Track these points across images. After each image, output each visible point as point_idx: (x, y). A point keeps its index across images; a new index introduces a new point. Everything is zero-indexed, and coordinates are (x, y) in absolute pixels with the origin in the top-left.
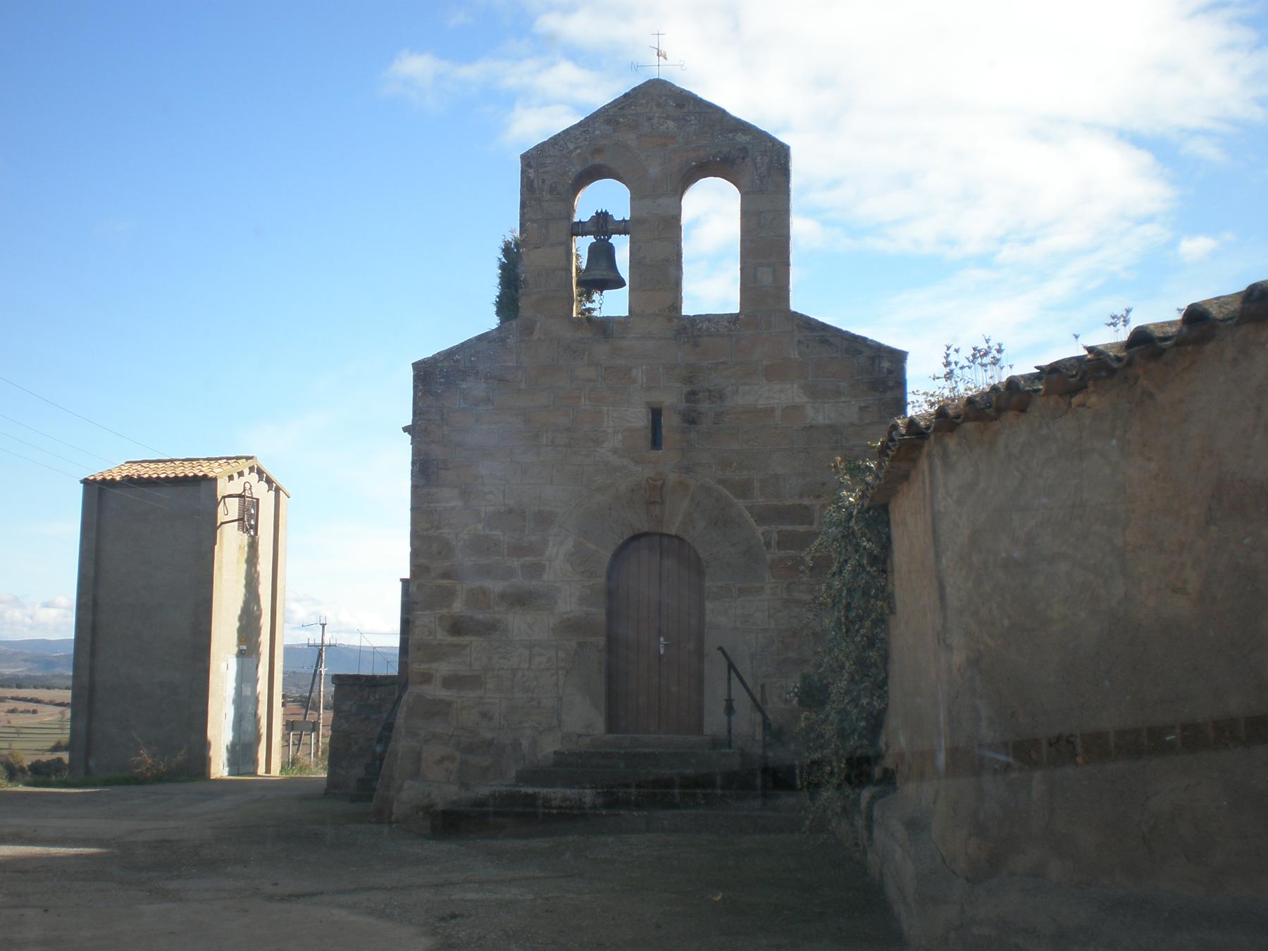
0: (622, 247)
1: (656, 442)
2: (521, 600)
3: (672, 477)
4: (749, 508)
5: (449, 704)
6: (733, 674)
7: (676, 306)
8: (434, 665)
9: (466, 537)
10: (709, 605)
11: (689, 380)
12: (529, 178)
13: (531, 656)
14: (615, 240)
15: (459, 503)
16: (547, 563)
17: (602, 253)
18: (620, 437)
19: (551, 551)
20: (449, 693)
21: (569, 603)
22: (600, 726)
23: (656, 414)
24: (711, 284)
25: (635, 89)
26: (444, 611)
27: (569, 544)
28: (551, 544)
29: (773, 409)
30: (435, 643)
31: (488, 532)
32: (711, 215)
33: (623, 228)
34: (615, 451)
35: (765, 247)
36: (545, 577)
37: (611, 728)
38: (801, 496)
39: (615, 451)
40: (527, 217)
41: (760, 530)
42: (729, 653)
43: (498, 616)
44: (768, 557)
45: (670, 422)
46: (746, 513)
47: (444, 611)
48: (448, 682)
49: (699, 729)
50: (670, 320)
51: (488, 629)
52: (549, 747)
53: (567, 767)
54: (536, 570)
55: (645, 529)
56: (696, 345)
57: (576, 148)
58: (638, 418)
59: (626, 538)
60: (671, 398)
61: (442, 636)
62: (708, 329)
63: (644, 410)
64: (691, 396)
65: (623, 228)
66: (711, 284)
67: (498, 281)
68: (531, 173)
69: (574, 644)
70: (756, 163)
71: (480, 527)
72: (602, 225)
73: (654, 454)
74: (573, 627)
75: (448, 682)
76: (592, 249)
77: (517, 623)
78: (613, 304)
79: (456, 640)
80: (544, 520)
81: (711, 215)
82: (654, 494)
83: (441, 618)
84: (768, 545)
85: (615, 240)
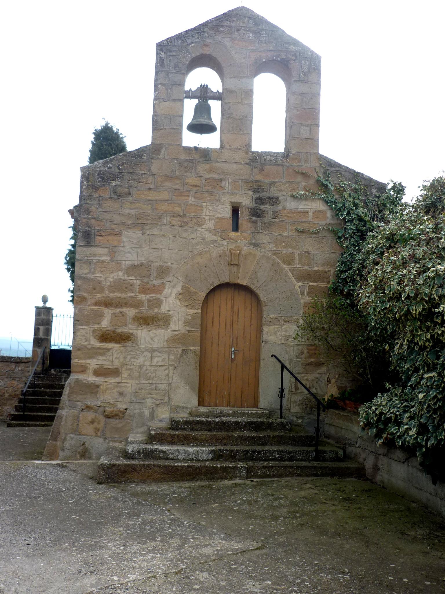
0: (216, 107)
1: (236, 227)
2: (145, 321)
3: (245, 250)
4: (292, 271)
5: (98, 386)
6: (285, 370)
7: (249, 145)
8: (89, 361)
9: (111, 280)
10: (265, 329)
11: (256, 190)
12: (161, 58)
13: (152, 357)
14: (211, 102)
15: (108, 258)
17: (203, 109)
18: (213, 222)
19: (167, 291)
20: (98, 379)
21: (177, 326)
22: (195, 401)
23: (236, 211)
24: (268, 135)
25: (229, 11)
26: (96, 327)
27: (178, 289)
28: (167, 287)
29: (307, 212)
30: (89, 347)
31: (126, 277)
32: (269, 95)
33: (217, 97)
34: (210, 231)
35: (303, 117)
36: (162, 308)
37: (201, 403)
38: (323, 265)
39: (210, 231)
40: (159, 82)
41: (298, 284)
42: (279, 358)
43: (131, 331)
44: (302, 301)
45: (243, 214)
46: (290, 274)
47: (96, 327)
48: (98, 373)
49: (256, 405)
50: (247, 153)
51: (123, 339)
52: (164, 415)
53: (181, 431)
54: (157, 303)
55: (227, 281)
56: (262, 170)
57: (192, 43)
58: (227, 212)
59: (215, 285)
60: (246, 200)
61: (94, 342)
62: (270, 160)
63: (229, 207)
64: (259, 200)
65: (217, 97)
66: (268, 135)
67: (90, 146)
68: (163, 55)
69: (180, 350)
70: (297, 66)
71: (121, 273)
72: (204, 94)
73: (233, 234)
74: (178, 339)
75: (98, 373)
76: (197, 107)
77: (144, 335)
78: (211, 141)
79: (103, 345)
80: (163, 271)
81: (269, 95)
82: (234, 260)
83: (94, 331)
84: (303, 293)
85: (211, 102)
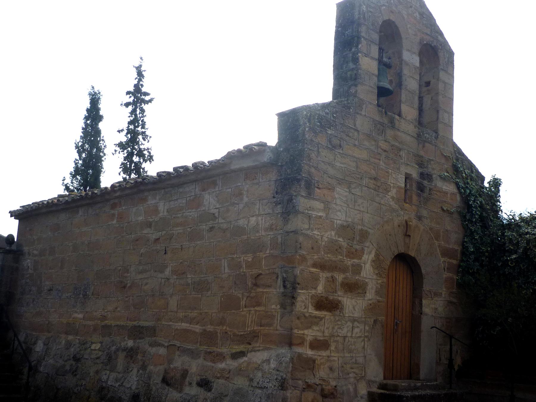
4: (439, 246)
16: (363, 265)
69: (372, 320)
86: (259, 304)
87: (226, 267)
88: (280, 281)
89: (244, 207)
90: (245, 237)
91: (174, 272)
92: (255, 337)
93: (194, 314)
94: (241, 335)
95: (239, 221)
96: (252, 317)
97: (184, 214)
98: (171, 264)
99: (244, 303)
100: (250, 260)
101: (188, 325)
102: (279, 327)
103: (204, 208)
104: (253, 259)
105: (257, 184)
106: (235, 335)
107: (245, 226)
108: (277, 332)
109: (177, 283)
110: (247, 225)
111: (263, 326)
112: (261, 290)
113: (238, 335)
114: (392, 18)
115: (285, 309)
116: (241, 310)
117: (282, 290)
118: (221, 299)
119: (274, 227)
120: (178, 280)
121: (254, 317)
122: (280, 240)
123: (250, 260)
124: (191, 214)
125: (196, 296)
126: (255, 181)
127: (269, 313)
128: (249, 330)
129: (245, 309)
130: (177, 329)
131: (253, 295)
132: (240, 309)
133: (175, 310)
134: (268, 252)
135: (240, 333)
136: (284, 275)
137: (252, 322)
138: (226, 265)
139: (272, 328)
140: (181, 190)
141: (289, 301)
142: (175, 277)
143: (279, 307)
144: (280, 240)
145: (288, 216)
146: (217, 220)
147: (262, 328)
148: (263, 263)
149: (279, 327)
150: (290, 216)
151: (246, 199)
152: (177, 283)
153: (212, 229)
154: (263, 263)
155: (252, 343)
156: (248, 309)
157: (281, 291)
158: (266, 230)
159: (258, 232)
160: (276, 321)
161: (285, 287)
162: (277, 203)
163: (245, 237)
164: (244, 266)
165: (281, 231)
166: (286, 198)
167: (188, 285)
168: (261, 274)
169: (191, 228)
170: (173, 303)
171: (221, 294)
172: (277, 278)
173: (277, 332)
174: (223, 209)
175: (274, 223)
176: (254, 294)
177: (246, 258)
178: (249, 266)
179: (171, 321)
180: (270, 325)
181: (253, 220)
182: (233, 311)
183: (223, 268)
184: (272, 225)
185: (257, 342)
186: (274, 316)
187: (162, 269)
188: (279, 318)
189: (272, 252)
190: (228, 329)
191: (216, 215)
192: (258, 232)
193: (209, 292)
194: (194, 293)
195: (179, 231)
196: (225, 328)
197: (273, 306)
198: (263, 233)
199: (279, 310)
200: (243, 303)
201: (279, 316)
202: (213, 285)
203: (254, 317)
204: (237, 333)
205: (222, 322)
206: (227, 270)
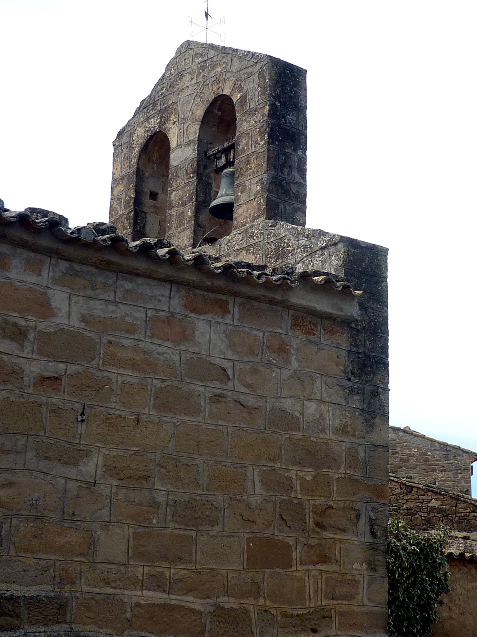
86: (325, 559)
87: (257, 483)
88: (363, 524)
89: (291, 377)
90: (298, 435)
91: (112, 470)
92: (324, 617)
93: (178, 571)
94: (298, 615)
95: (283, 400)
96: (316, 582)
97: (142, 345)
98: (104, 451)
99: (298, 556)
100: (309, 478)
101: (166, 596)
102: (366, 602)
103: (196, 349)
104: (315, 477)
105: (317, 344)
106: (285, 615)
107: (297, 414)
108: (364, 609)
109: (120, 496)
110: (302, 413)
111: (337, 599)
112: (332, 536)
113: (292, 616)
114: (236, 97)
115: (375, 571)
116: (294, 569)
117: (368, 539)
118: (248, 546)
119: (349, 429)
120: (124, 491)
121: (319, 584)
122: (362, 454)
123: (309, 478)
124: (160, 350)
125: (181, 532)
126: (312, 338)
127: (348, 577)
128: (312, 605)
129: (299, 568)
130: (138, 605)
131: (313, 542)
132: (291, 567)
133: (122, 558)
134: (342, 470)
135: (295, 612)
136: (372, 514)
137: (316, 592)
138: (257, 479)
139: (354, 602)
140: (128, 286)
141: (380, 558)
142: (115, 482)
143: (365, 566)
144: (362, 454)
145: (374, 418)
146: (230, 384)
147: (335, 602)
148: (335, 489)
149: (366, 602)
150: (376, 420)
151: (295, 364)
152: (120, 496)
153: (218, 398)
154: (335, 489)
155: (319, 629)
156: (305, 567)
157: (366, 540)
158: (337, 431)
159: (323, 430)
160: (360, 591)
161: (373, 534)
162: (352, 392)
163: (298, 435)
164: (298, 488)
165: (362, 441)
166: (368, 388)
167: (155, 505)
168: (331, 507)
169: (163, 381)
170: (114, 543)
171: (246, 536)
172: (358, 516)
173: (364, 609)
174: (243, 366)
175: (349, 423)
176: (317, 542)
177: (301, 474)
178: (307, 489)
179: (108, 584)
180: (351, 597)
181: (312, 407)
182: (278, 570)
183: (249, 484)
184: (345, 426)
185: (329, 626)
186: (357, 582)
187: (74, 455)
188: (365, 586)
189: (348, 471)
190: (268, 603)
191: (230, 372)
192: (323, 430)
193: (217, 529)
194: (172, 525)
195: (128, 379)
196: (261, 601)
197: (356, 566)
198: (332, 437)
199: (365, 573)
200: (296, 555)
201: (365, 583)
202: (227, 514)
203: (319, 584)
204: (290, 611)
205: (255, 591)
206: (258, 489)
